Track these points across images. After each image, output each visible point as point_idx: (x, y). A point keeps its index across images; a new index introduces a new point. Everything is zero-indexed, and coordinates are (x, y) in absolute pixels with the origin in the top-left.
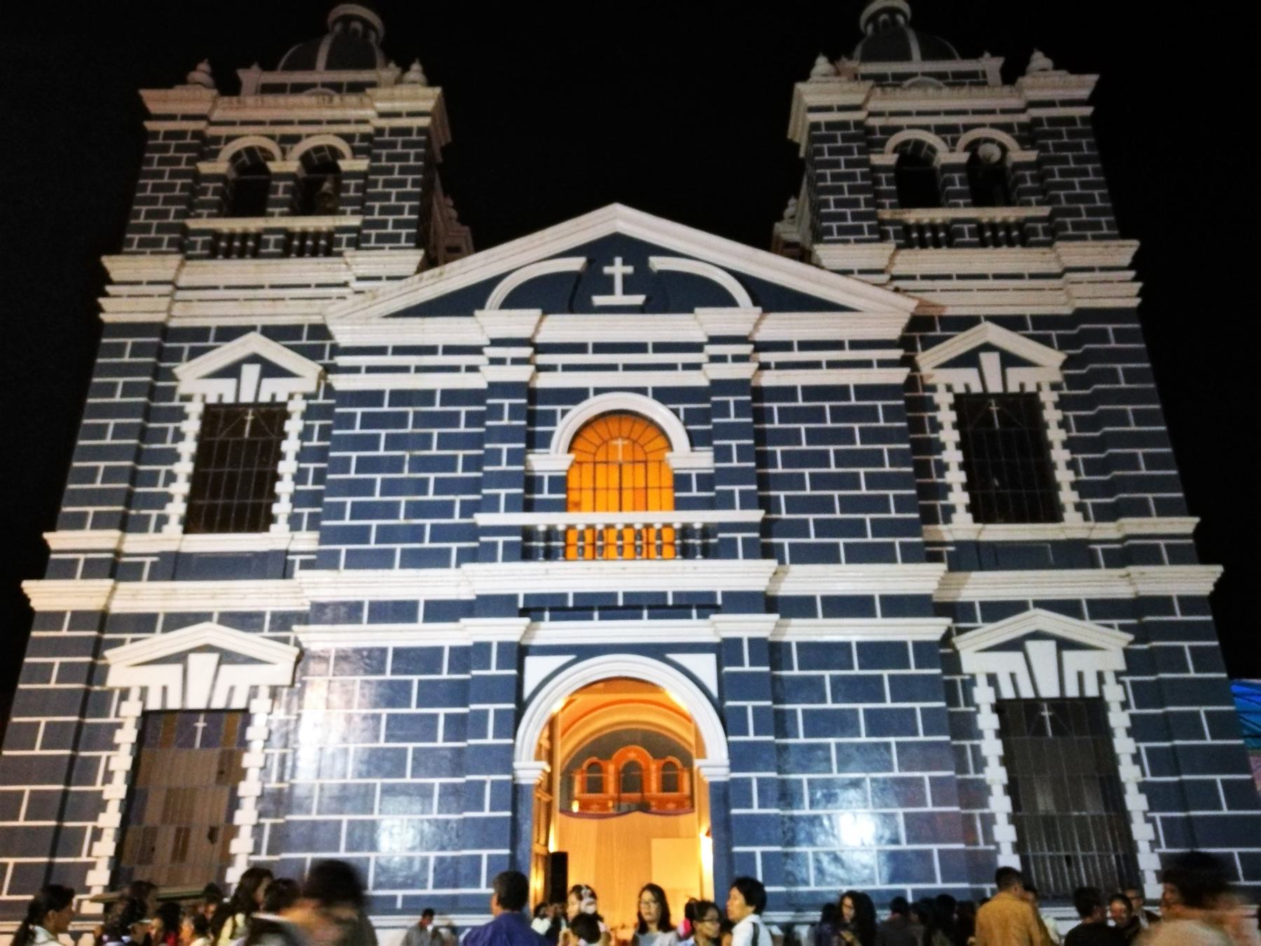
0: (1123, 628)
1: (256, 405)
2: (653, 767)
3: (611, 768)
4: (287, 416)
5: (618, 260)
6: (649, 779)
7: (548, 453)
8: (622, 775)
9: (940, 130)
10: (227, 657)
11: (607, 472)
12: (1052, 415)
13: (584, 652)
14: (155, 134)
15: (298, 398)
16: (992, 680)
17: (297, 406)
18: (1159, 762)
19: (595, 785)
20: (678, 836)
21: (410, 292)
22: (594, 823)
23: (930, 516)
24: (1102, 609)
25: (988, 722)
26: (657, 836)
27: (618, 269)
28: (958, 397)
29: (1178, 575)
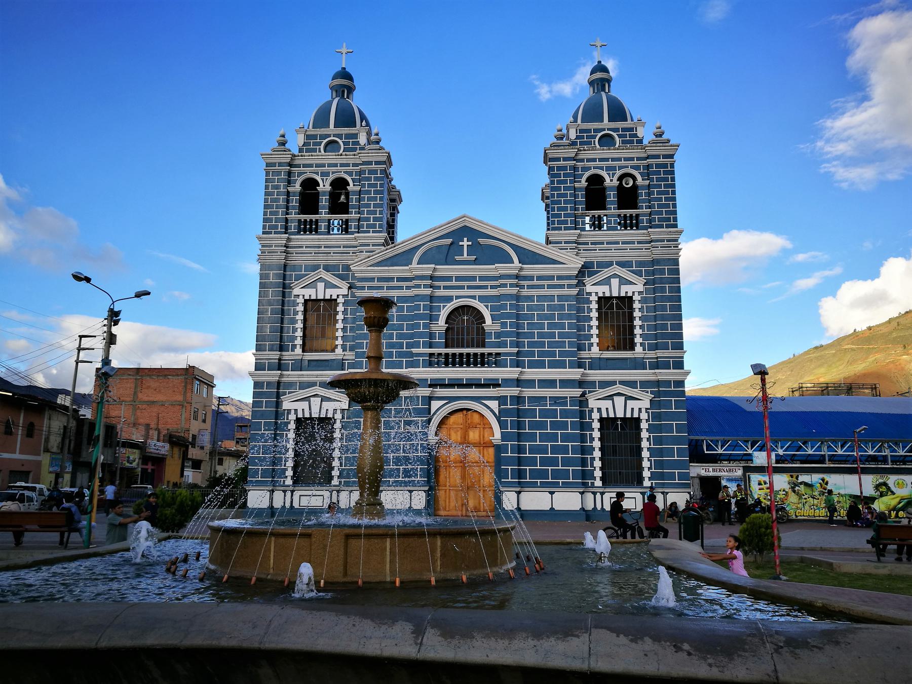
0: (652, 393)
1: (619, 298)
4: (337, 305)
5: (465, 239)
9: (609, 169)
10: (324, 399)
12: (637, 305)
13: (451, 399)
15: (636, 294)
16: (599, 410)
17: (636, 297)
18: (658, 440)
20: (598, 408)
23: (580, 348)
24: (645, 385)
25: (596, 425)
27: (465, 243)
28: (599, 298)
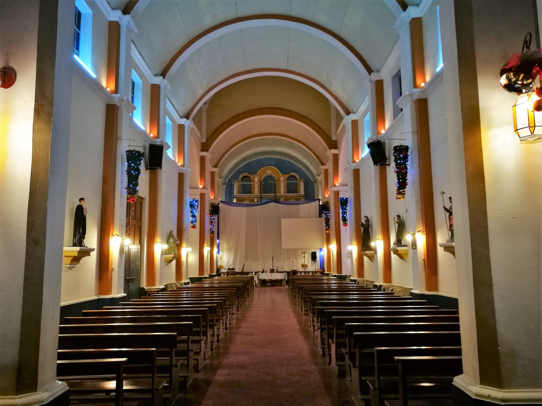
2: (282, 179)
3: (256, 179)
6: (280, 186)
14: (225, 334)
19: (247, 189)
20: (298, 217)
22: (245, 209)
29: (431, 89)
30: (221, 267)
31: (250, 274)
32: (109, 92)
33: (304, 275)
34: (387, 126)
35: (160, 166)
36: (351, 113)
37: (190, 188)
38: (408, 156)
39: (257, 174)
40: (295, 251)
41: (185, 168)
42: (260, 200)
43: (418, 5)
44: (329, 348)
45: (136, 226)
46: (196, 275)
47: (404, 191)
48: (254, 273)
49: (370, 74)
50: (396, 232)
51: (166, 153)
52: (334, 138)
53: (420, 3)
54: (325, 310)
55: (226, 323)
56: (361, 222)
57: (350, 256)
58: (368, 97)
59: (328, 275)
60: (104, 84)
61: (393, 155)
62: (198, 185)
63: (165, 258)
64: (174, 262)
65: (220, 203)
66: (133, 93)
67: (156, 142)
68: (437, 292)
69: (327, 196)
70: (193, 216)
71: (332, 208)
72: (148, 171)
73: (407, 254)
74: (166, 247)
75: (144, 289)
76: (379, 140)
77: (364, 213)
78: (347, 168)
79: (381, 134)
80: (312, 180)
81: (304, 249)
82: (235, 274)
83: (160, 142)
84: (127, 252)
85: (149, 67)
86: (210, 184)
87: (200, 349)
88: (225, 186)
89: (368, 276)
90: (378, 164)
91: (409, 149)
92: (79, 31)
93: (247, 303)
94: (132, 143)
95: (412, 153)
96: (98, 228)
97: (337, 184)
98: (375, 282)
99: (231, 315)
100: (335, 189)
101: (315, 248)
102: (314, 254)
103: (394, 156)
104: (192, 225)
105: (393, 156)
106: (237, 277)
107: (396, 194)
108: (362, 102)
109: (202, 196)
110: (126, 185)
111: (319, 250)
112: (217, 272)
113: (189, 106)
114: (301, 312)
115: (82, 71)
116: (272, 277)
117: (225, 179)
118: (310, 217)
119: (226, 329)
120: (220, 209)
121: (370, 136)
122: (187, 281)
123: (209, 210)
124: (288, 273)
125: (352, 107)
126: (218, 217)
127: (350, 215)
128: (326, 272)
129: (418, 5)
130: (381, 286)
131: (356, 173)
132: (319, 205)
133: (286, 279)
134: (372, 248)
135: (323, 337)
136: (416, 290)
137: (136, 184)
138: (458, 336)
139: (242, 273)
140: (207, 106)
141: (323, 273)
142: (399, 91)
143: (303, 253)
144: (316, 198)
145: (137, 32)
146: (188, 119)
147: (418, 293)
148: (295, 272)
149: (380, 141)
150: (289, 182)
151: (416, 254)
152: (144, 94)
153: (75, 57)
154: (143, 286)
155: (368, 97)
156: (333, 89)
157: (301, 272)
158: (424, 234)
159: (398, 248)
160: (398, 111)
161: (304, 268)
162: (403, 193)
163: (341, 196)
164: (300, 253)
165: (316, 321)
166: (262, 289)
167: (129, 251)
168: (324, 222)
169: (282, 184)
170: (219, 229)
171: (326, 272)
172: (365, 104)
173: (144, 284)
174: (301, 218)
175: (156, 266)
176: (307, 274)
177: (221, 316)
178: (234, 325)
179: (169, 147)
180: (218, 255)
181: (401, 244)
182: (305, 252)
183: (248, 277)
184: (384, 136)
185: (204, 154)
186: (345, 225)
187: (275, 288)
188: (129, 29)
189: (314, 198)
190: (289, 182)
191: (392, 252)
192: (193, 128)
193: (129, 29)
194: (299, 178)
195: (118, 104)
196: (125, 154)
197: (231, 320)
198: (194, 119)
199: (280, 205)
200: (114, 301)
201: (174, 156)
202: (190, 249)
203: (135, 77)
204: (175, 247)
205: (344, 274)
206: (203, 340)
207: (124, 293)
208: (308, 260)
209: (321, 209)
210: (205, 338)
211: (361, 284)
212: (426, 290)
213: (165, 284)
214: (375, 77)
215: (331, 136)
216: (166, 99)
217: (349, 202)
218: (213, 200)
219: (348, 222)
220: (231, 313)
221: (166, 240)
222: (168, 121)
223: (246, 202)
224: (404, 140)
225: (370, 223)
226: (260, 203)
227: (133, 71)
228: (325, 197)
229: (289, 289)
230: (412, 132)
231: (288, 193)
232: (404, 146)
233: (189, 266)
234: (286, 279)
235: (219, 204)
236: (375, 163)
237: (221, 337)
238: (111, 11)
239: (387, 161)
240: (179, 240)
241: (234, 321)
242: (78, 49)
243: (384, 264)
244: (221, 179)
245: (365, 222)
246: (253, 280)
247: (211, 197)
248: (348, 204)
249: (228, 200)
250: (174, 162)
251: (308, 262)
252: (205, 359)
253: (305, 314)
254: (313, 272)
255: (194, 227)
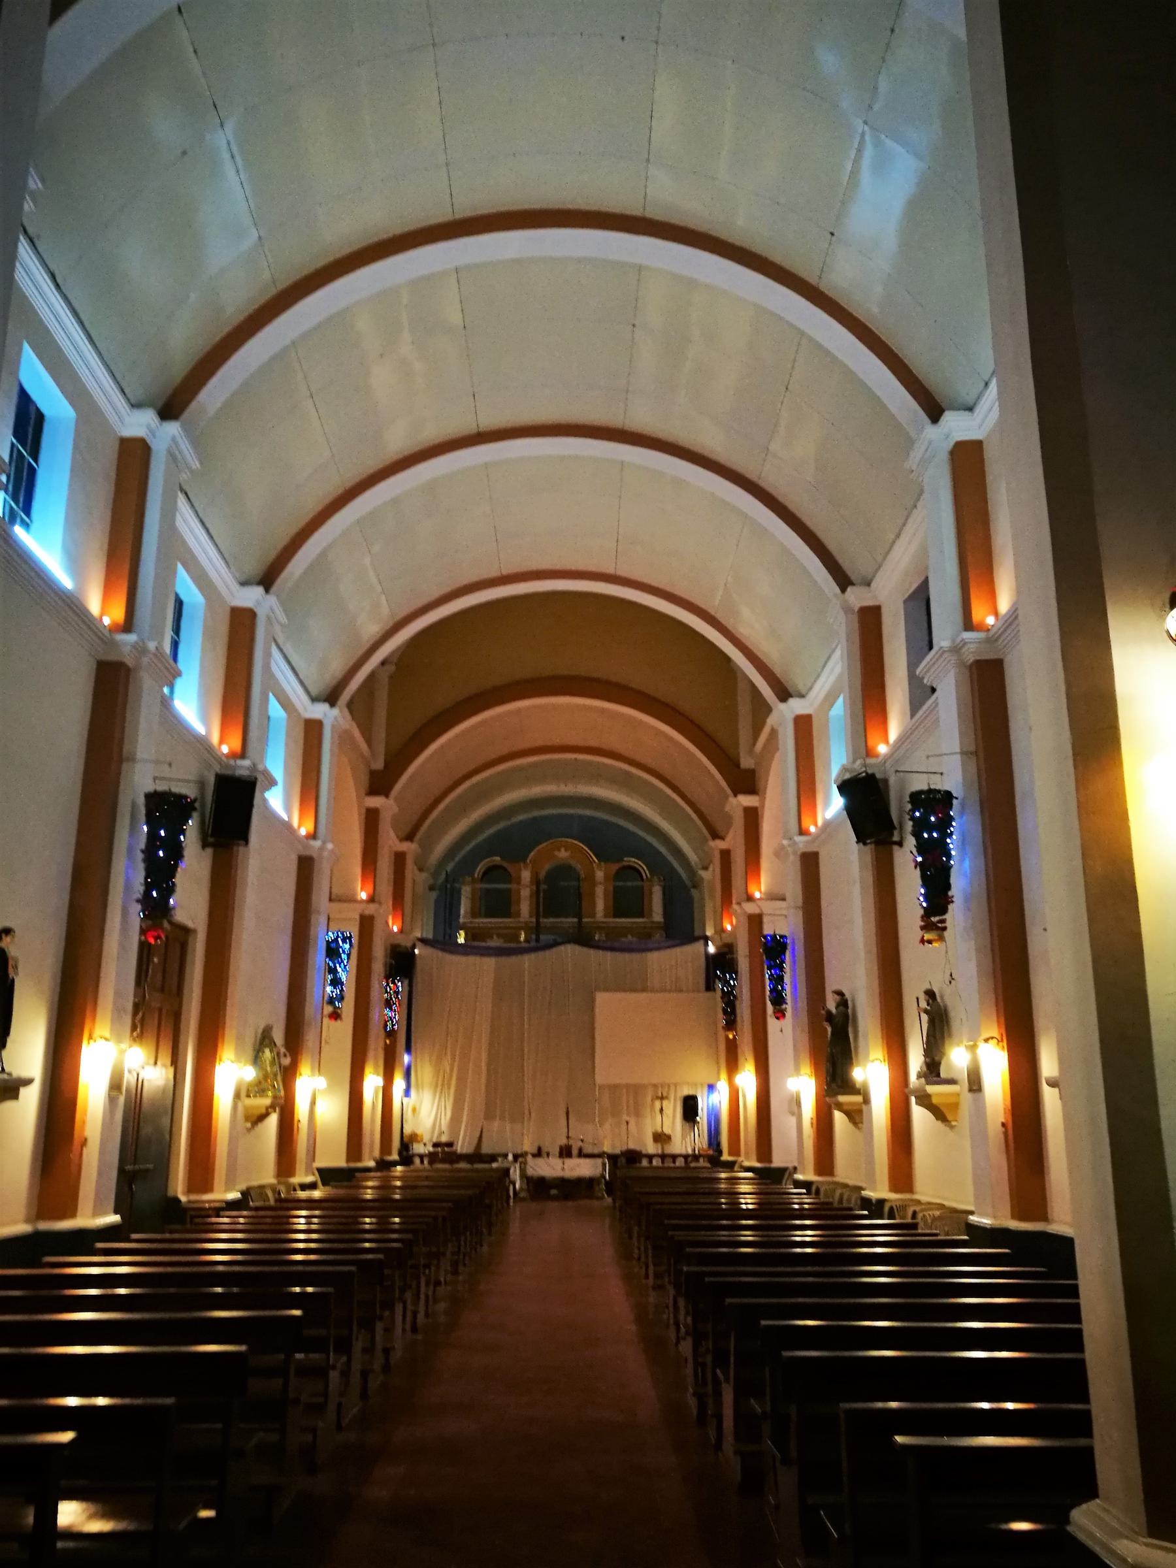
2: (600, 875)
3: (526, 875)
6: (592, 894)
7: (129, 415)
8: (543, 887)
11: (188, 781)
20: (644, 989)
21: (28, 275)
22: (490, 962)
26: (600, 990)
30: (414, 1137)
31: (500, 1159)
32: (108, 628)
33: (660, 1164)
34: (893, 734)
35: (244, 836)
36: (791, 696)
37: (330, 900)
38: (951, 819)
39: (528, 861)
40: (636, 1090)
41: (317, 844)
42: (534, 937)
43: (970, 409)
44: (718, 1394)
45: (164, 1011)
46: (339, 1160)
47: (943, 921)
48: (510, 1157)
49: (843, 590)
50: (925, 1038)
51: (265, 801)
52: (746, 762)
53: (975, 404)
54: (707, 1279)
55: (415, 1313)
56: (824, 1009)
57: (795, 1109)
58: (838, 653)
59: (730, 1166)
60: (94, 605)
61: (909, 817)
62: (354, 890)
63: (246, 1109)
64: (273, 1120)
65: (419, 944)
66: (177, 630)
67: (235, 767)
68: (1046, 1223)
69: (729, 928)
70: (336, 982)
71: (743, 964)
72: (209, 851)
73: (955, 1106)
74: (249, 1073)
75: (178, 1201)
76: (870, 771)
77: (832, 982)
78: (783, 847)
79: (877, 756)
80: (688, 883)
81: (662, 1086)
82: (454, 1158)
83: (248, 768)
84: (134, 1091)
85: (224, 558)
86: (391, 888)
87: (326, 1395)
88: (434, 895)
89: (844, 1172)
90: (869, 841)
91: (955, 802)
92: (36, 462)
93: (485, 1248)
94: (166, 772)
95: (963, 806)
96: (50, 1011)
97: (757, 895)
98: (864, 1190)
99: (431, 1287)
100: (750, 908)
101: (695, 1085)
102: (692, 1102)
103: (913, 818)
104: (328, 1009)
105: (910, 819)
106: (460, 1170)
107: (919, 929)
108: (824, 666)
109: (367, 924)
110: (139, 888)
111: (706, 1089)
112: (400, 1154)
113: (337, 667)
114: (644, 1281)
115: (33, 569)
116: (563, 1169)
117: (435, 874)
118: (681, 991)
119: (414, 1329)
120: (419, 964)
121: (844, 761)
122: (309, 1179)
123: (385, 965)
124: (613, 1158)
125: (796, 678)
126: (410, 986)
127: (795, 987)
128: (726, 1157)
129: (970, 409)
130: (881, 1202)
131: (810, 863)
132: (707, 954)
133: (607, 1177)
134: (858, 1086)
135: (700, 1360)
136: (982, 1215)
137: (170, 890)
138: (1080, 1368)
139: (476, 1157)
140: (391, 668)
141: (715, 1160)
142: (927, 638)
143: (657, 1098)
144: (697, 933)
145: (195, 464)
146: (332, 705)
147: (988, 1227)
148: (633, 1157)
149: (873, 775)
150: (620, 884)
151: (980, 1109)
152: (209, 635)
153: (18, 530)
154: (176, 1192)
155: (838, 653)
156: (743, 631)
157: (650, 1157)
158: (1003, 1047)
159: (931, 1089)
160: (921, 693)
161: (659, 1146)
162: (940, 925)
163: (768, 930)
164: (649, 1099)
165: (682, 1312)
166: (534, 1206)
167: (140, 1086)
168: (720, 1005)
169: (600, 891)
170: (413, 1018)
171: (726, 1157)
172: (832, 670)
173: (179, 1189)
174: (652, 991)
175: (216, 1133)
176: (669, 1163)
177: (397, 1291)
178: (442, 1319)
179: (272, 783)
180: (406, 1100)
181: (938, 1075)
182: (665, 1094)
183: (492, 1170)
184: (885, 762)
185: (375, 802)
186: (780, 1014)
187: (570, 1203)
188: (173, 457)
189: (693, 931)
190: (620, 884)
191: (913, 1099)
192: (346, 732)
193: (173, 457)
194: (647, 872)
195: (130, 662)
196: (141, 801)
197: (431, 1303)
198: (350, 705)
199: (592, 952)
200: (83, 1241)
201: (288, 809)
202: (320, 1082)
203: (185, 586)
204: (275, 1075)
205: (777, 1162)
206: (334, 1368)
207: (116, 1212)
208: (671, 1119)
209: (711, 965)
210: (344, 1359)
211: (826, 1195)
212: (1013, 1217)
213: (243, 1187)
214: (857, 597)
215: (739, 761)
216: (270, 646)
217: (789, 947)
218: (400, 936)
219: (789, 1007)
220: (432, 1281)
221: (250, 1053)
222: (275, 709)
223: (495, 942)
224: (939, 776)
225: (850, 1011)
226: (533, 944)
227: (180, 569)
228: (723, 930)
229: (614, 1208)
230: (963, 753)
231: (615, 916)
232: (939, 791)
233: (318, 1130)
234: (605, 1178)
235: (414, 947)
236: (861, 838)
237: (397, 1355)
238: (128, 411)
239: (896, 833)
240: (288, 1054)
241: (442, 1306)
242: (27, 510)
243: (890, 1134)
244: (424, 875)
245: (837, 1008)
246: (507, 1179)
247: (393, 924)
248: (788, 954)
249: (441, 938)
250: (287, 826)
251: (673, 1122)
252: (339, 1428)
253: (654, 1288)
254: (686, 1157)
255: (336, 1016)
